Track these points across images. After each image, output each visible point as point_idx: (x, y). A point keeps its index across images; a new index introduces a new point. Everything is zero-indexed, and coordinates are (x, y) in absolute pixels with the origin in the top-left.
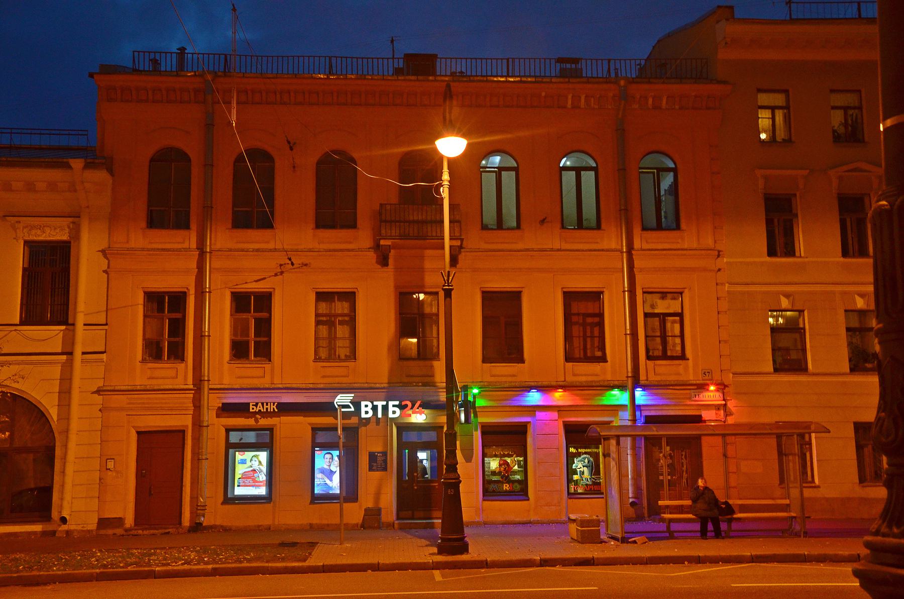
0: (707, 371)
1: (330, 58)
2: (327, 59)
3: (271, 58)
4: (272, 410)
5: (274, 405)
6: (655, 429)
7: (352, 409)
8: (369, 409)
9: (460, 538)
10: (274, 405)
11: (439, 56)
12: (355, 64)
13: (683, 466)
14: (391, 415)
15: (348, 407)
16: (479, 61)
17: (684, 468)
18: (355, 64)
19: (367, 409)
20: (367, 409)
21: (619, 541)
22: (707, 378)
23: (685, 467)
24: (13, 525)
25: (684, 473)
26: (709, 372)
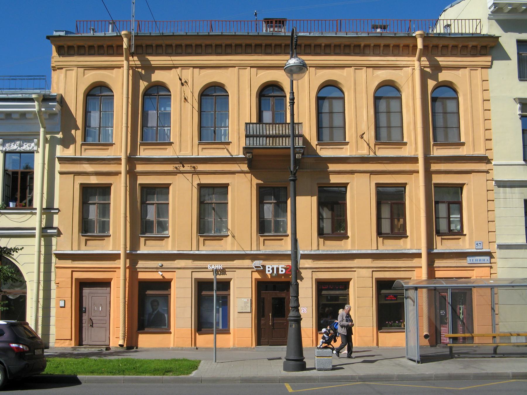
0: (479, 243)
1: (211, 21)
2: (209, 22)
3: (101, 22)
4: (220, 268)
5: (220, 266)
6: (443, 282)
7: (262, 268)
8: (270, 269)
9: (300, 359)
10: (220, 266)
11: (287, 19)
12: (463, 24)
13: (460, 310)
14: (280, 272)
15: (259, 267)
16: (467, 21)
17: (461, 311)
18: (463, 24)
19: (269, 269)
20: (269, 269)
21: (415, 362)
22: (479, 247)
23: (462, 310)
24: (495, 373)
25: (461, 315)
26: (480, 243)
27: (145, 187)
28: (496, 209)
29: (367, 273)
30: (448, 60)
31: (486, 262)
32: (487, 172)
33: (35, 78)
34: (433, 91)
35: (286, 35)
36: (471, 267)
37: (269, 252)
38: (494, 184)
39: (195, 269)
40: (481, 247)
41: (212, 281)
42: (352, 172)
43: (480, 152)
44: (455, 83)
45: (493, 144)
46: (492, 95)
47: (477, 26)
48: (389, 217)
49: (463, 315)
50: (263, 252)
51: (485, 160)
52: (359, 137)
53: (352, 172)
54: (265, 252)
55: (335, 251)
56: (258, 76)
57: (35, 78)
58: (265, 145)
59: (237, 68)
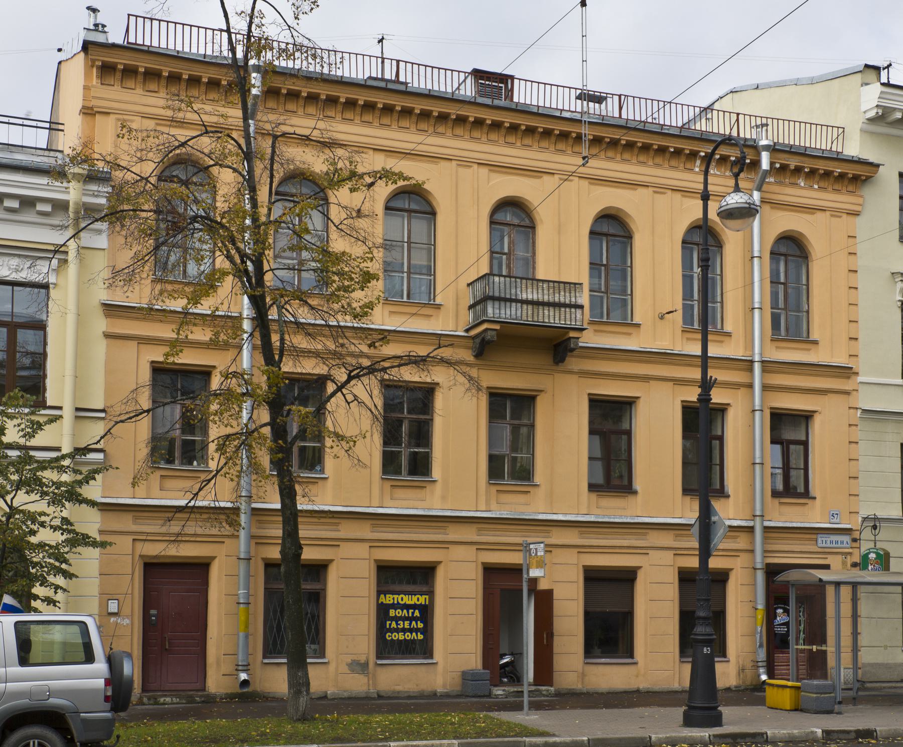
12: (209, 38)
22: (835, 520)
23: (802, 626)
25: (802, 633)
27: (298, 380)
28: (860, 458)
29: (362, 550)
30: (390, 137)
31: (845, 545)
32: (847, 393)
33: (12, 120)
34: (280, 184)
35: (540, 112)
36: (643, 551)
37: (507, 514)
38: (859, 416)
39: (374, 543)
40: (838, 521)
41: (519, 567)
42: (646, 379)
43: (840, 360)
44: (636, 219)
45: (861, 348)
46: (861, 262)
47: (731, 130)
48: (781, 466)
49: (804, 633)
50: (496, 514)
51: (846, 372)
52: (657, 316)
53: (646, 379)
54: (500, 514)
55: (523, 513)
56: (490, 184)
57: (12, 120)
58: (492, 315)
59: (454, 163)
